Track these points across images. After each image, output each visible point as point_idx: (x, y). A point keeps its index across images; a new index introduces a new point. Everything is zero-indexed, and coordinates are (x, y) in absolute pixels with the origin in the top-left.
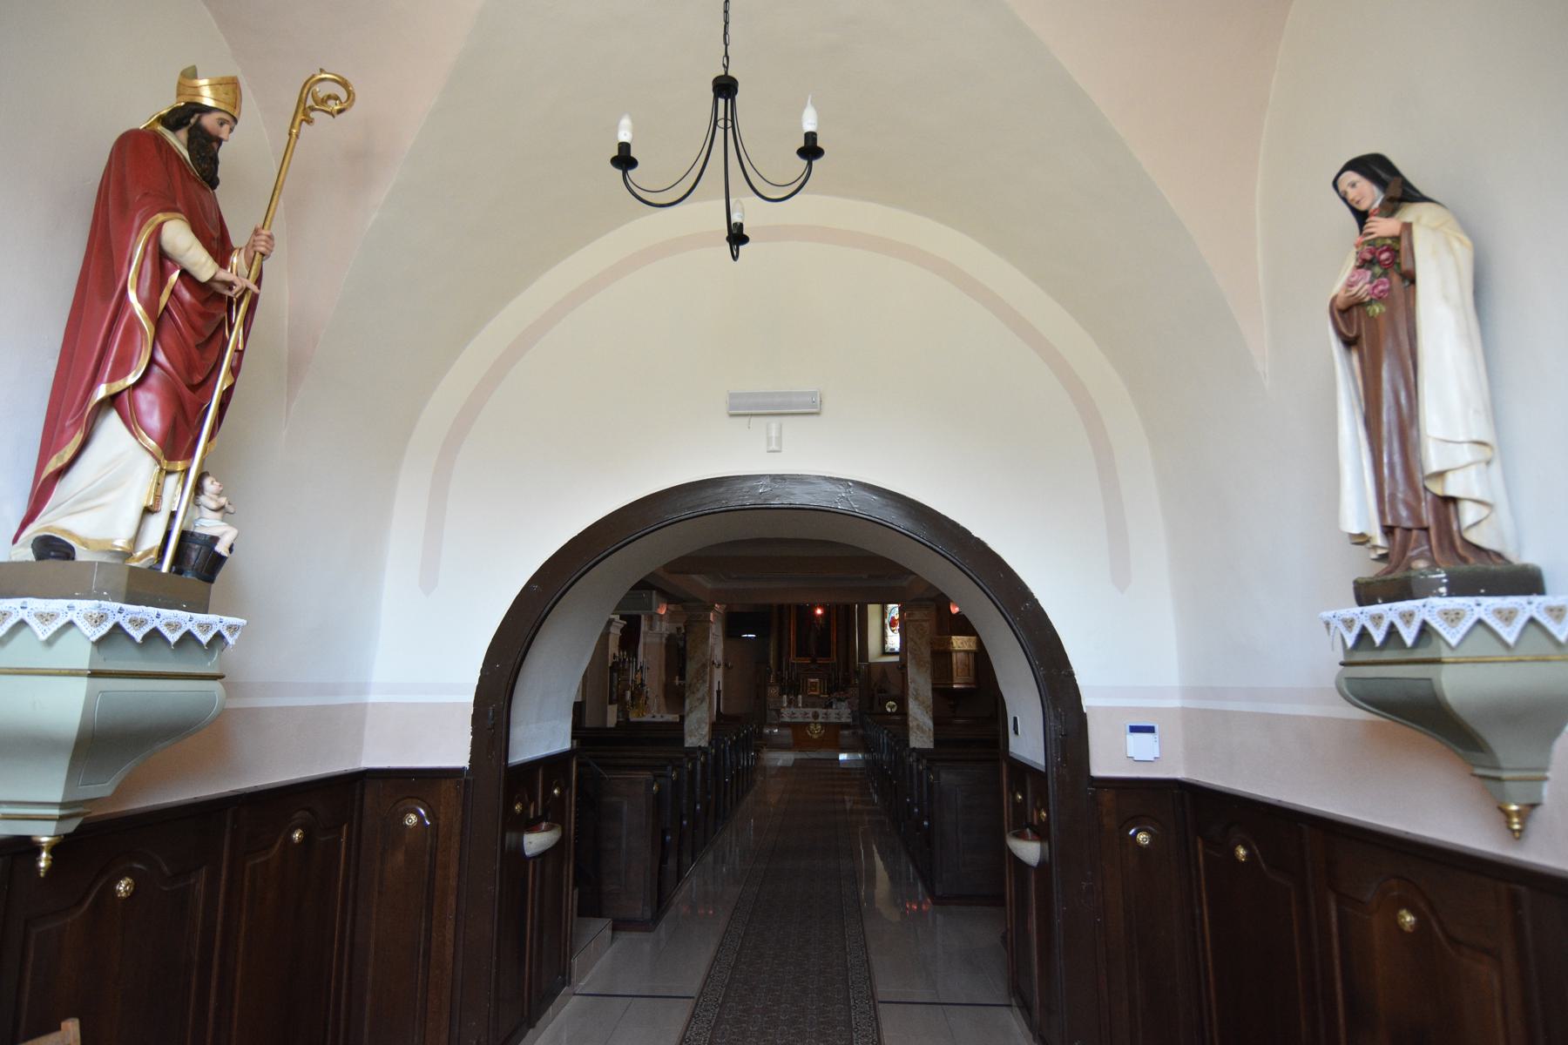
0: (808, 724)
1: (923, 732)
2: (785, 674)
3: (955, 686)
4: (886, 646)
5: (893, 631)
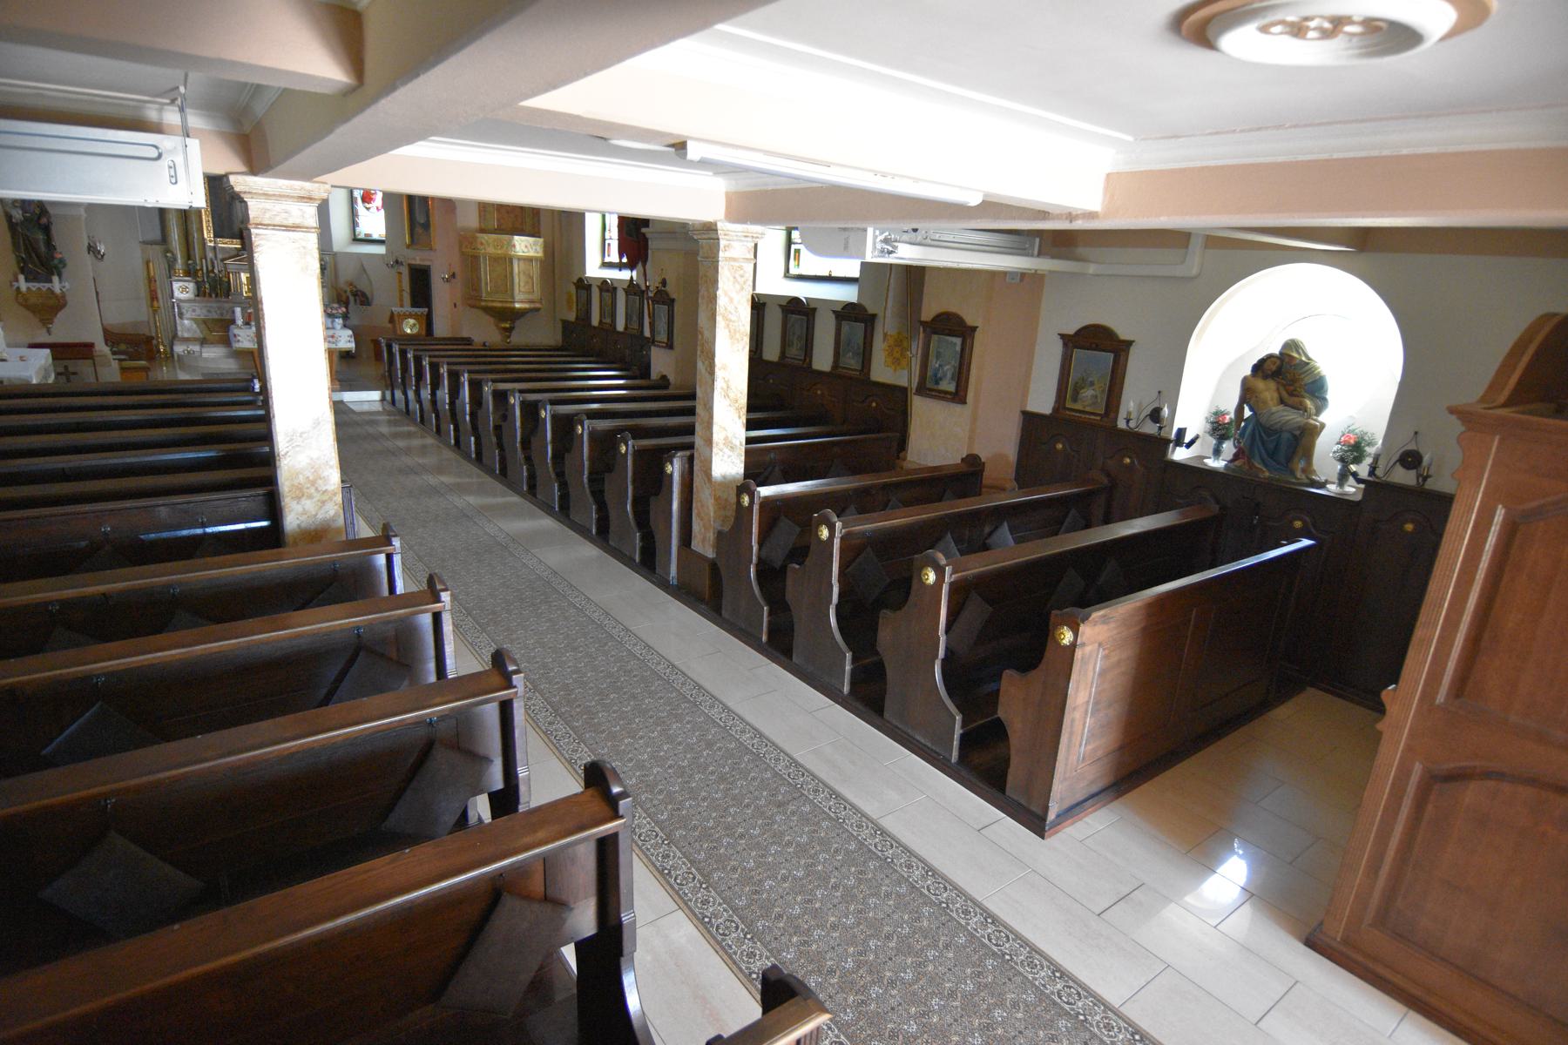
1: (732, 448)
3: (517, 305)
4: (358, 230)
5: (368, 209)
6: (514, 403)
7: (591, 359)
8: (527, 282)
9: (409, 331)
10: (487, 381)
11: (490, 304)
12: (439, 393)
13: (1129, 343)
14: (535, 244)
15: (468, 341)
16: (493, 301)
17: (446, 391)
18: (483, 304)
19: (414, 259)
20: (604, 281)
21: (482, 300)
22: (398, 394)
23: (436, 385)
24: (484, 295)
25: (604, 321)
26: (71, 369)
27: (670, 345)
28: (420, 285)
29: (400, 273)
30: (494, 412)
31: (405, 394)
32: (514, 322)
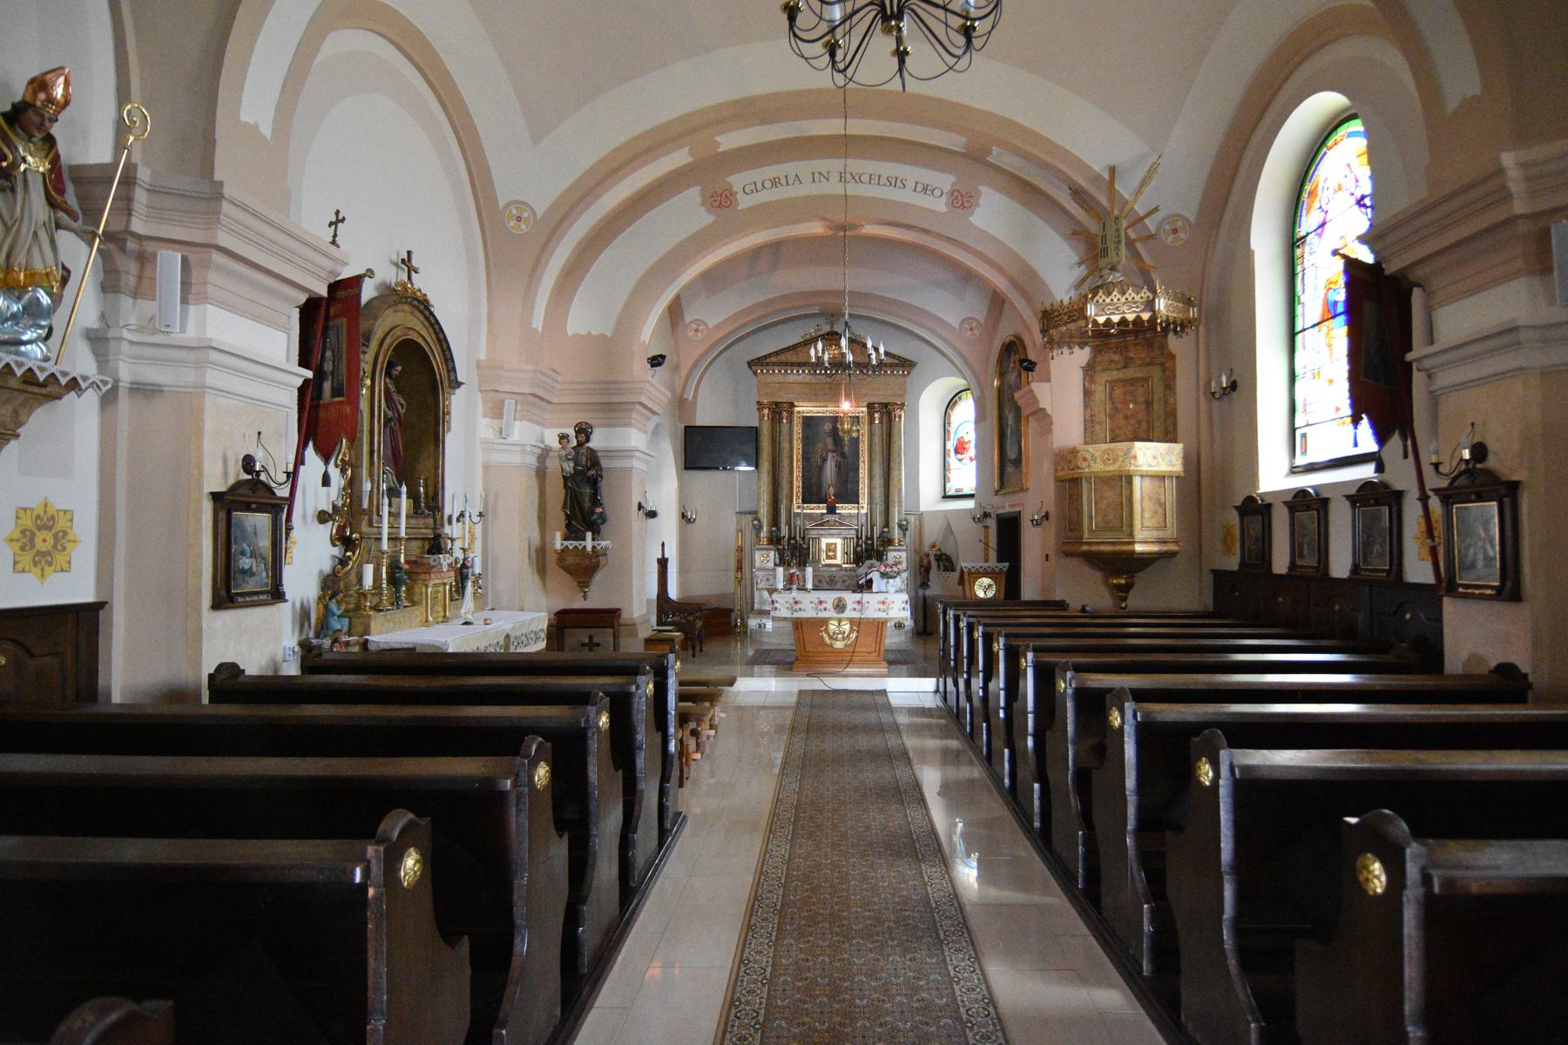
0: (825, 622)
2: (784, 531)
3: (1138, 548)
5: (960, 460)
6: (1121, 728)
7: (1278, 631)
8: (1155, 512)
9: (981, 594)
10: (1065, 669)
11: (1095, 548)
12: (992, 686)
13: (461, 384)
14: (1169, 453)
15: (1061, 605)
16: (1098, 543)
17: (1002, 685)
18: (1085, 548)
19: (1004, 507)
20: (1301, 493)
21: (1083, 543)
22: (950, 681)
23: (989, 674)
24: (1086, 535)
25: (1299, 562)
26: (596, 640)
27: (1510, 589)
28: (1008, 531)
29: (986, 527)
30: (1078, 739)
31: (956, 684)
32: (1133, 576)
